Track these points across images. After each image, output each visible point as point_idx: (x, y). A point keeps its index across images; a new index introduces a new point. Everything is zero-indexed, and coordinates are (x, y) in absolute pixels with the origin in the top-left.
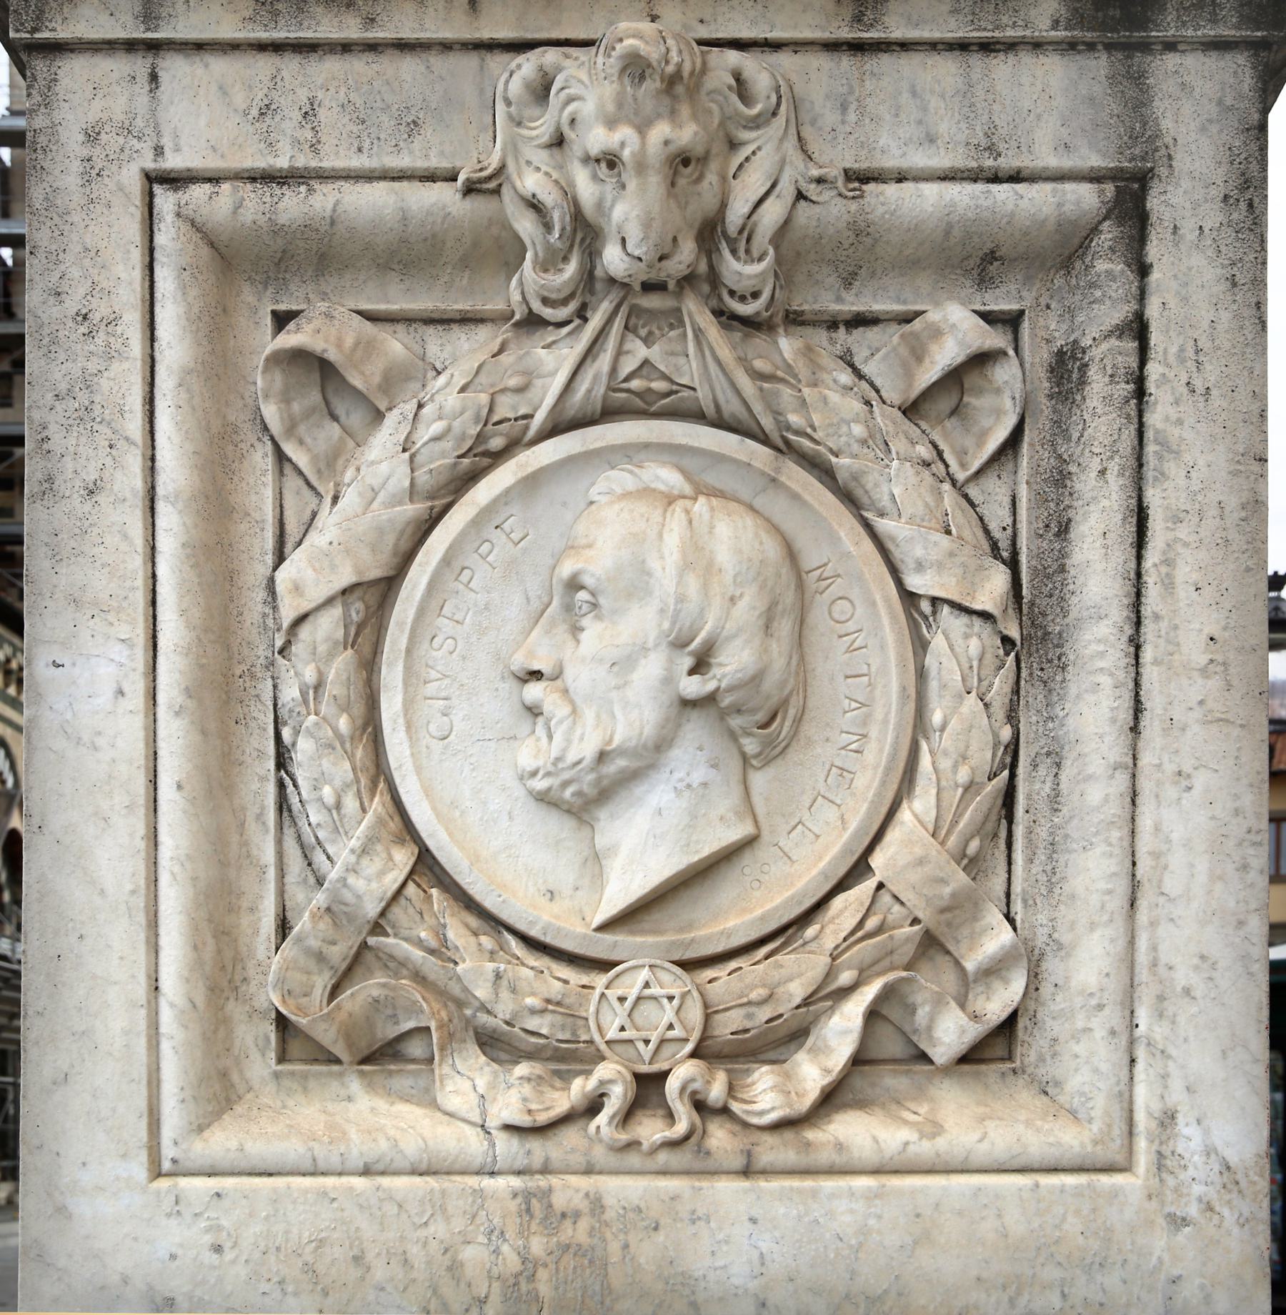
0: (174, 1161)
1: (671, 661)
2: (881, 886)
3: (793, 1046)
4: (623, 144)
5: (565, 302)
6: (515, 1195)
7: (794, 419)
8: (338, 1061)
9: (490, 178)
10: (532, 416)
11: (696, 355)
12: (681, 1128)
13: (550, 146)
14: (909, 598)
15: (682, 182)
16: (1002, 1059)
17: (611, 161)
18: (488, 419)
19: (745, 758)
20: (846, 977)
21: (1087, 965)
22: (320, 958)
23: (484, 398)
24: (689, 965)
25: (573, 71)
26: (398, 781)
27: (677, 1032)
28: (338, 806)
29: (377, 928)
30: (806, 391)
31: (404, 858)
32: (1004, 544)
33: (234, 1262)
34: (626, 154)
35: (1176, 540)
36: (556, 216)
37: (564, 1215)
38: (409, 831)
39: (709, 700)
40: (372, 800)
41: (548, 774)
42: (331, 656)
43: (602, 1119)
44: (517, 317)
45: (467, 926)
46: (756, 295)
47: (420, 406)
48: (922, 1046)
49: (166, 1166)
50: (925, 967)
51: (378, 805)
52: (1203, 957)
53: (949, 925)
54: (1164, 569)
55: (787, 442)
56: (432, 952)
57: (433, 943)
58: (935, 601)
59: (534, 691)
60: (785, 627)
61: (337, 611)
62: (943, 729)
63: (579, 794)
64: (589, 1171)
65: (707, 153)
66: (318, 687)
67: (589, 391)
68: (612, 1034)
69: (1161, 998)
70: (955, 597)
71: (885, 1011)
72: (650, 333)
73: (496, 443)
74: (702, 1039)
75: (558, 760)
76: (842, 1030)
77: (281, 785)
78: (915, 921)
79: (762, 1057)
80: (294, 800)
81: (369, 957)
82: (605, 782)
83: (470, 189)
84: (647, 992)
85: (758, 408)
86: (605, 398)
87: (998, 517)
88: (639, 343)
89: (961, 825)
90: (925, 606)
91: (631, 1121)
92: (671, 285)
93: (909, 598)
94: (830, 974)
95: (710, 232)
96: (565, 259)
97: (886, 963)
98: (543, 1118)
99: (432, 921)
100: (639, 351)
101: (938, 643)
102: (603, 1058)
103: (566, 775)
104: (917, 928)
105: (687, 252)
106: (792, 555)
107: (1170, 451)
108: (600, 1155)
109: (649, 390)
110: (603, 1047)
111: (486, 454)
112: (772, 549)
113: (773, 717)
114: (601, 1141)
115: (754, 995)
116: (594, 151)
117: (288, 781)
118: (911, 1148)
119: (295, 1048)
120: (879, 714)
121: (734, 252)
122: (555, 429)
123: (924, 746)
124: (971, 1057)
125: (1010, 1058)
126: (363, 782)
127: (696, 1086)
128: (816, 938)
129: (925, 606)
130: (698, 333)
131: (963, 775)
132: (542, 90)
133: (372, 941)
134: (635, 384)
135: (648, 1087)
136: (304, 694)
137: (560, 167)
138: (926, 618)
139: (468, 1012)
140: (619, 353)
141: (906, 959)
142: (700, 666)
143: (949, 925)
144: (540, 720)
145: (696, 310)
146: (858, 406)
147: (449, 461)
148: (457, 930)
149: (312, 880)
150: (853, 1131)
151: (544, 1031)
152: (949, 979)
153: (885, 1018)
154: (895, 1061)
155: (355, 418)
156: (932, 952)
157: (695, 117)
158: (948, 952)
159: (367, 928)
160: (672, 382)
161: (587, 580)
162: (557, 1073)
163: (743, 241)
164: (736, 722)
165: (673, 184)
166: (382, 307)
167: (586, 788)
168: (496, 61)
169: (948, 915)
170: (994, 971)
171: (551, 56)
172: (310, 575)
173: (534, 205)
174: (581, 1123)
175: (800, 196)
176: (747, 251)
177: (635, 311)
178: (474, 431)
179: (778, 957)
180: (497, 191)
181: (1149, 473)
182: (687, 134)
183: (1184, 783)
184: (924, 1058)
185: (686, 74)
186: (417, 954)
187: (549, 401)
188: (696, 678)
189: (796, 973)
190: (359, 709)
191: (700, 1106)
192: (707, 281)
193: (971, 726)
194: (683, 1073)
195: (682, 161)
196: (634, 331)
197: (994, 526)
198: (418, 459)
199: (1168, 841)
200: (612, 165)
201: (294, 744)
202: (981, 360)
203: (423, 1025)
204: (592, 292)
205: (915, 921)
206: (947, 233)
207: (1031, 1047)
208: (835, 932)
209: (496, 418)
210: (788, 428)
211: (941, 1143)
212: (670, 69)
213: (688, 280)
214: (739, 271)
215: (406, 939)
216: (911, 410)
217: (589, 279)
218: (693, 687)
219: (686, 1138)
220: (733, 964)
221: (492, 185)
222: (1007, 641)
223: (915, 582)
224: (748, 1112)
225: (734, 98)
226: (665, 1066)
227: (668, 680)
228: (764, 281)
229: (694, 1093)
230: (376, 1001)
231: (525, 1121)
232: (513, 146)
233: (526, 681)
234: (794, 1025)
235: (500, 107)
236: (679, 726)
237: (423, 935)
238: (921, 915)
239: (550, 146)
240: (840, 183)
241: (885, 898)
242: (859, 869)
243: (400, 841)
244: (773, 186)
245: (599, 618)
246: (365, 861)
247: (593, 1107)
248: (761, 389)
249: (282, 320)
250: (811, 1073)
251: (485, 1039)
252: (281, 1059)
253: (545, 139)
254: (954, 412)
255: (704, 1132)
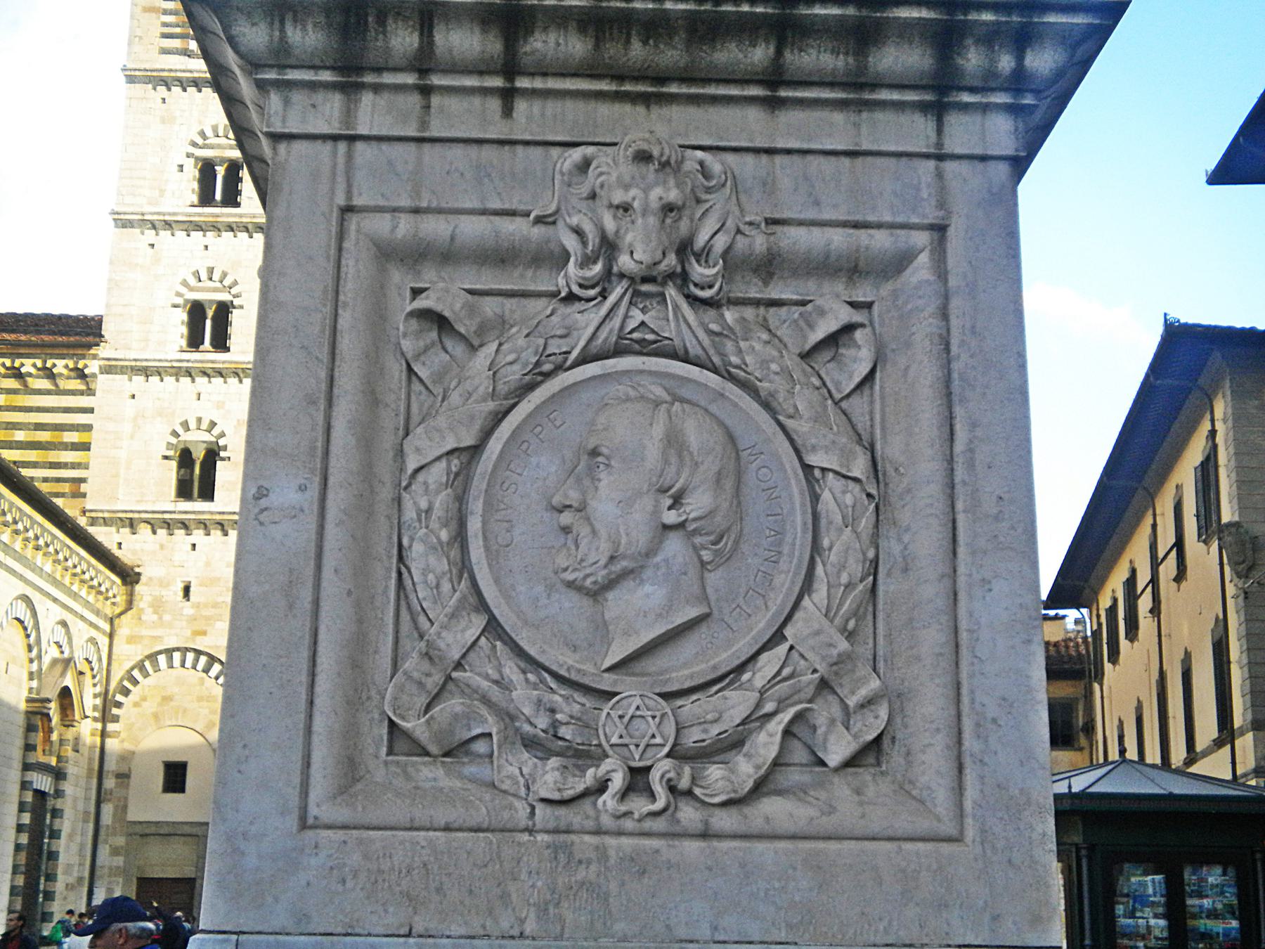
0: (316, 818)
1: (657, 501)
2: (792, 648)
3: (734, 752)
4: (634, 199)
5: (593, 287)
6: (548, 847)
7: (734, 359)
8: (427, 754)
9: (550, 215)
10: (569, 353)
11: (675, 319)
12: (660, 804)
13: (587, 199)
14: (807, 468)
15: (668, 221)
16: (872, 765)
17: (626, 208)
18: (544, 355)
19: (703, 564)
20: (769, 707)
21: (930, 705)
22: (420, 684)
23: (541, 341)
24: (666, 696)
25: (603, 159)
26: (476, 571)
27: (658, 740)
28: (438, 586)
29: (459, 666)
30: (742, 344)
31: (479, 622)
32: (865, 437)
33: (354, 889)
34: (636, 204)
35: (975, 437)
36: (590, 237)
37: (580, 862)
38: (482, 605)
39: (681, 526)
40: (459, 583)
41: (575, 570)
42: (438, 492)
43: (606, 796)
44: (563, 294)
45: (519, 667)
46: (711, 287)
47: (500, 345)
48: (820, 754)
49: (310, 821)
50: (820, 701)
51: (464, 584)
52: (1004, 699)
53: (836, 674)
54: (968, 455)
55: (729, 373)
56: (496, 682)
57: (496, 676)
58: (823, 470)
59: (566, 518)
60: (729, 484)
61: (443, 464)
62: (830, 549)
63: (595, 583)
64: (598, 832)
65: (684, 205)
66: (428, 511)
67: (606, 339)
68: (615, 740)
69: (978, 725)
70: (838, 469)
71: (795, 729)
72: (645, 306)
73: (547, 367)
74: (674, 745)
75: (582, 560)
76: (766, 743)
77: (400, 574)
78: (815, 671)
79: (716, 759)
80: (408, 582)
81: (451, 686)
82: (613, 576)
83: (539, 220)
84: (638, 713)
85: (711, 352)
86: (616, 343)
87: (862, 422)
88: (638, 312)
89: (842, 612)
90: (817, 473)
91: (626, 799)
92: (659, 279)
93: (807, 468)
94: (758, 705)
95: (684, 248)
96: (595, 262)
97: (796, 697)
98: (568, 794)
99: (496, 663)
100: (637, 316)
101: (826, 496)
102: (607, 756)
103: (588, 571)
104: (816, 675)
105: (672, 260)
106: (731, 438)
107: (970, 385)
108: (607, 821)
109: (644, 340)
110: (607, 748)
111: (541, 374)
112: (719, 434)
113: (722, 537)
114: (606, 811)
115: (709, 717)
116: (616, 202)
117: (403, 570)
118: (815, 822)
119: (400, 745)
120: (789, 539)
121: (698, 261)
122: (583, 360)
123: (818, 560)
124: (852, 762)
125: (879, 764)
126: (454, 571)
127: (672, 775)
128: (749, 680)
129: (817, 473)
130: (676, 308)
131: (844, 579)
132: (584, 166)
133: (454, 675)
134: (635, 335)
135: (638, 779)
136: (419, 516)
137: (593, 211)
138: (818, 481)
139: (517, 724)
140: (626, 317)
141: (809, 696)
142: (677, 502)
143: (836, 674)
144: (570, 536)
145: (671, 292)
146: (775, 353)
147: (517, 377)
148: (511, 670)
149: (416, 635)
150: (772, 808)
151: (568, 737)
152: (836, 711)
153: (795, 735)
154: (802, 765)
155: (458, 349)
156: (825, 692)
157: (678, 186)
158: (835, 693)
159: (453, 665)
160: (658, 334)
161: (604, 450)
162: (577, 766)
163: (703, 256)
164: (698, 540)
165: (663, 221)
166: (478, 287)
167: (599, 579)
168: (555, 152)
169: (835, 668)
170: (868, 703)
171: (590, 150)
172: (426, 445)
173: (578, 232)
174: (592, 798)
175: (739, 231)
176: (706, 261)
177: (636, 293)
178: (534, 360)
179: (725, 693)
180: (554, 223)
181: (955, 399)
182: (673, 195)
183: (987, 587)
184: (822, 763)
185: (672, 162)
186: (485, 684)
187: (582, 343)
188: (673, 511)
189: (736, 704)
190: (454, 525)
191: (672, 789)
192: (682, 278)
193: (848, 549)
194: (662, 769)
195: (668, 208)
196: (635, 305)
197: (859, 427)
198: (498, 375)
199: (979, 623)
200: (626, 210)
201: (410, 547)
202: (849, 328)
203: (487, 731)
204: (609, 281)
205: (815, 671)
206: (827, 257)
207: (895, 758)
208: (763, 677)
209: (548, 352)
210: (730, 364)
211: (834, 819)
212: (664, 159)
213: (671, 276)
214: (699, 271)
215: (479, 674)
216: (806, 356)
217: (608, 274)
218: (671, 517)
219: (664, 810)
220: (694, 697)
221: (550, 220)
222: (869, 495)
223: (812, 459)
224: (706, 795)
225: (700, 176)
226: (649, 763)
227: (656, 512)
228: (716, 280)
229: (669, 780)
230: (456, 714)
231: (556, 796)
232: (564, 198)
233: (561, 512)
234: (735, 738)
235: (558, 177)
236: (661, 542)
237: (490, 672)
238: (818, 667)
239: (587, 199)
240: (763, 225)
241: (794, 654)
242: (778, 637)
243: (477, 610)
244: (723, 225)
245: (610, 474)
246: (454, 621)
247: (602, 787)
248: (713, 341)
249: (416, 292)
250: (745, 769)
251: (527, 742)
252: (390, 752)
253: (585, 195)
254: (832, 359)
255: (676, 807)
